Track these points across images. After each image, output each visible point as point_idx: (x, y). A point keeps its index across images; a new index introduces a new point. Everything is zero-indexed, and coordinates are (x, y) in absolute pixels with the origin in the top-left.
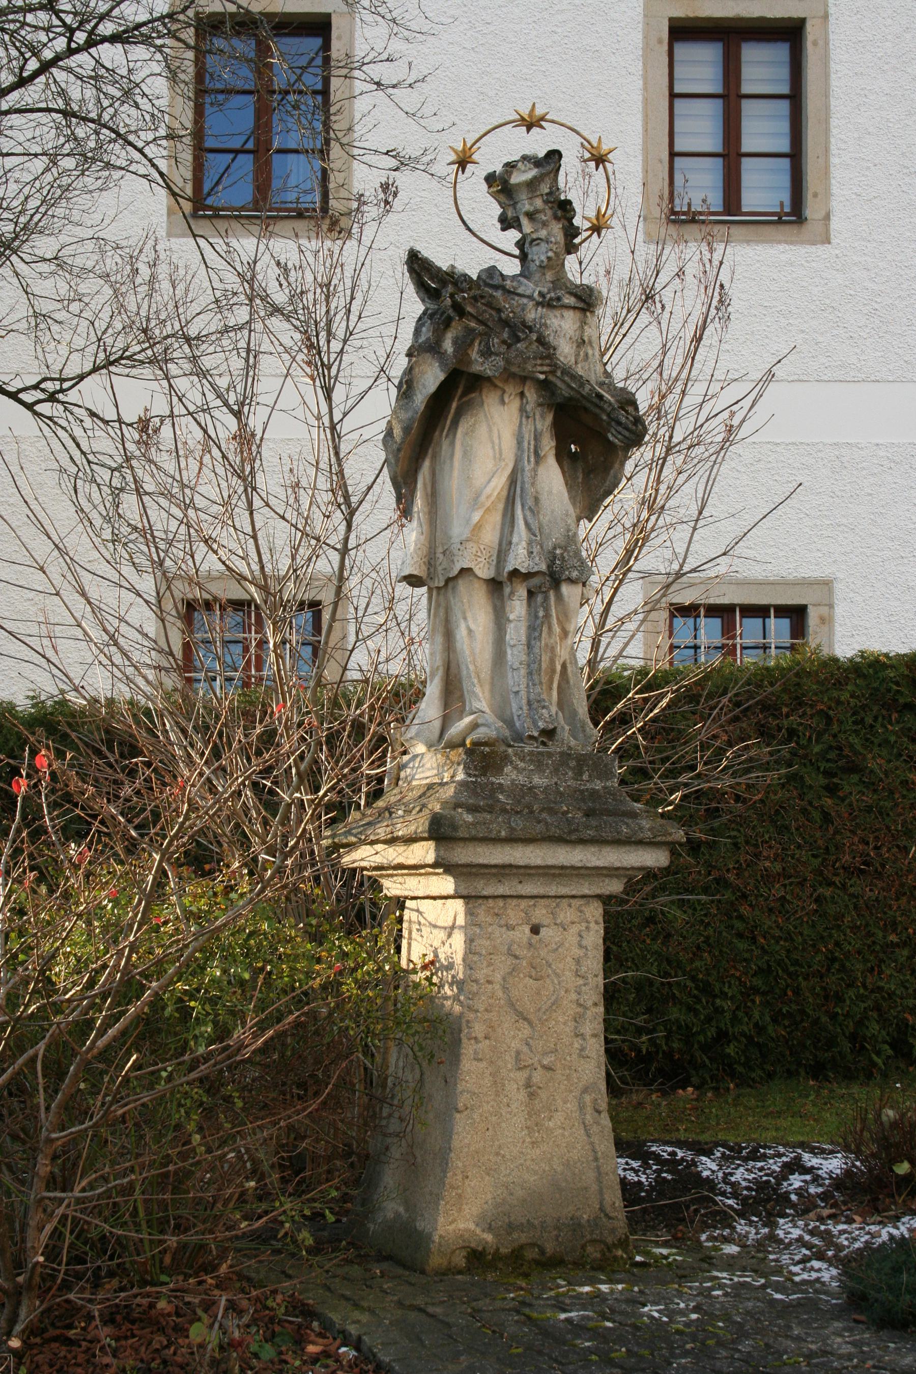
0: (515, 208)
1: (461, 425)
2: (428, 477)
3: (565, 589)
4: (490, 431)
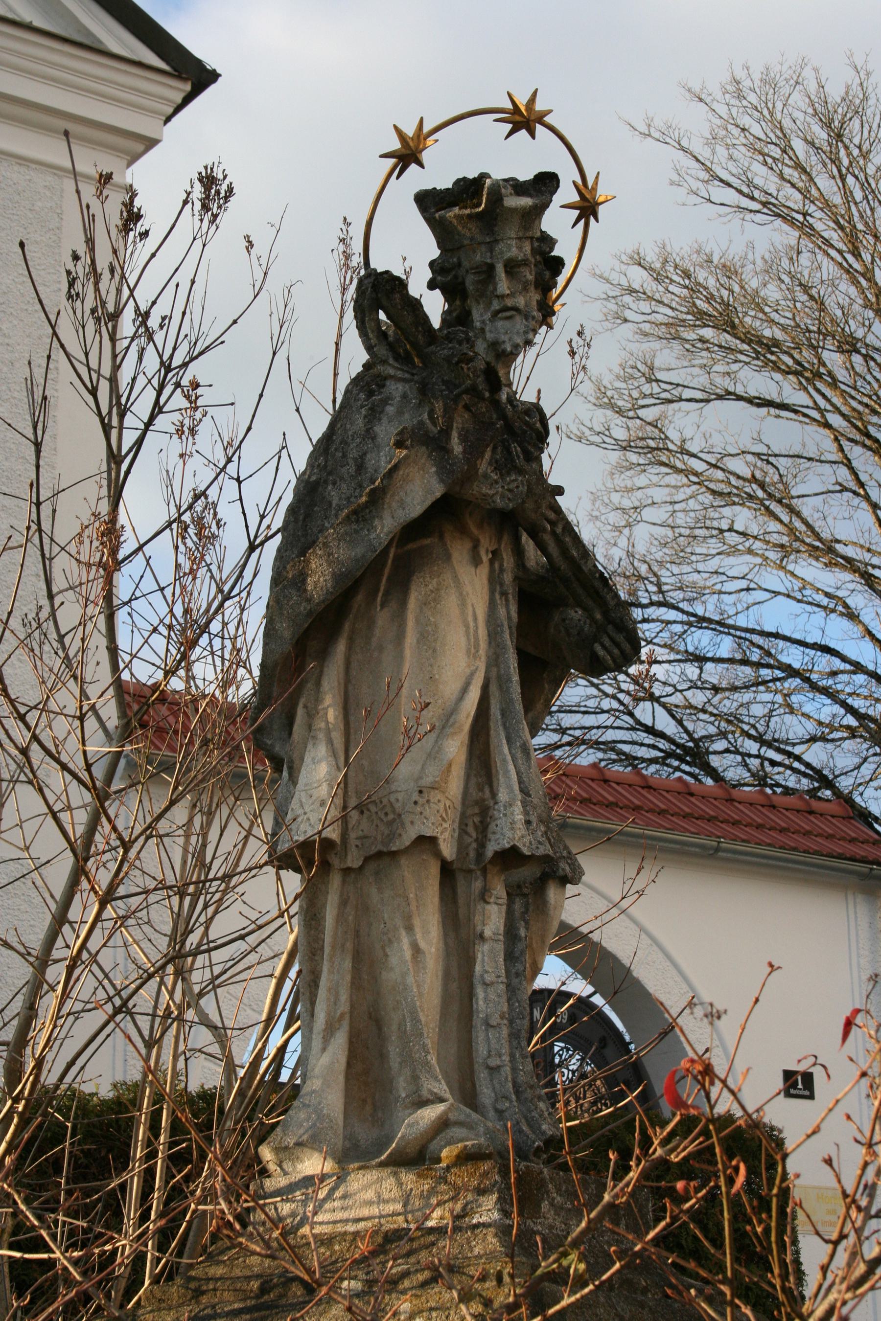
0: (491, 251)
4: (463, 604)
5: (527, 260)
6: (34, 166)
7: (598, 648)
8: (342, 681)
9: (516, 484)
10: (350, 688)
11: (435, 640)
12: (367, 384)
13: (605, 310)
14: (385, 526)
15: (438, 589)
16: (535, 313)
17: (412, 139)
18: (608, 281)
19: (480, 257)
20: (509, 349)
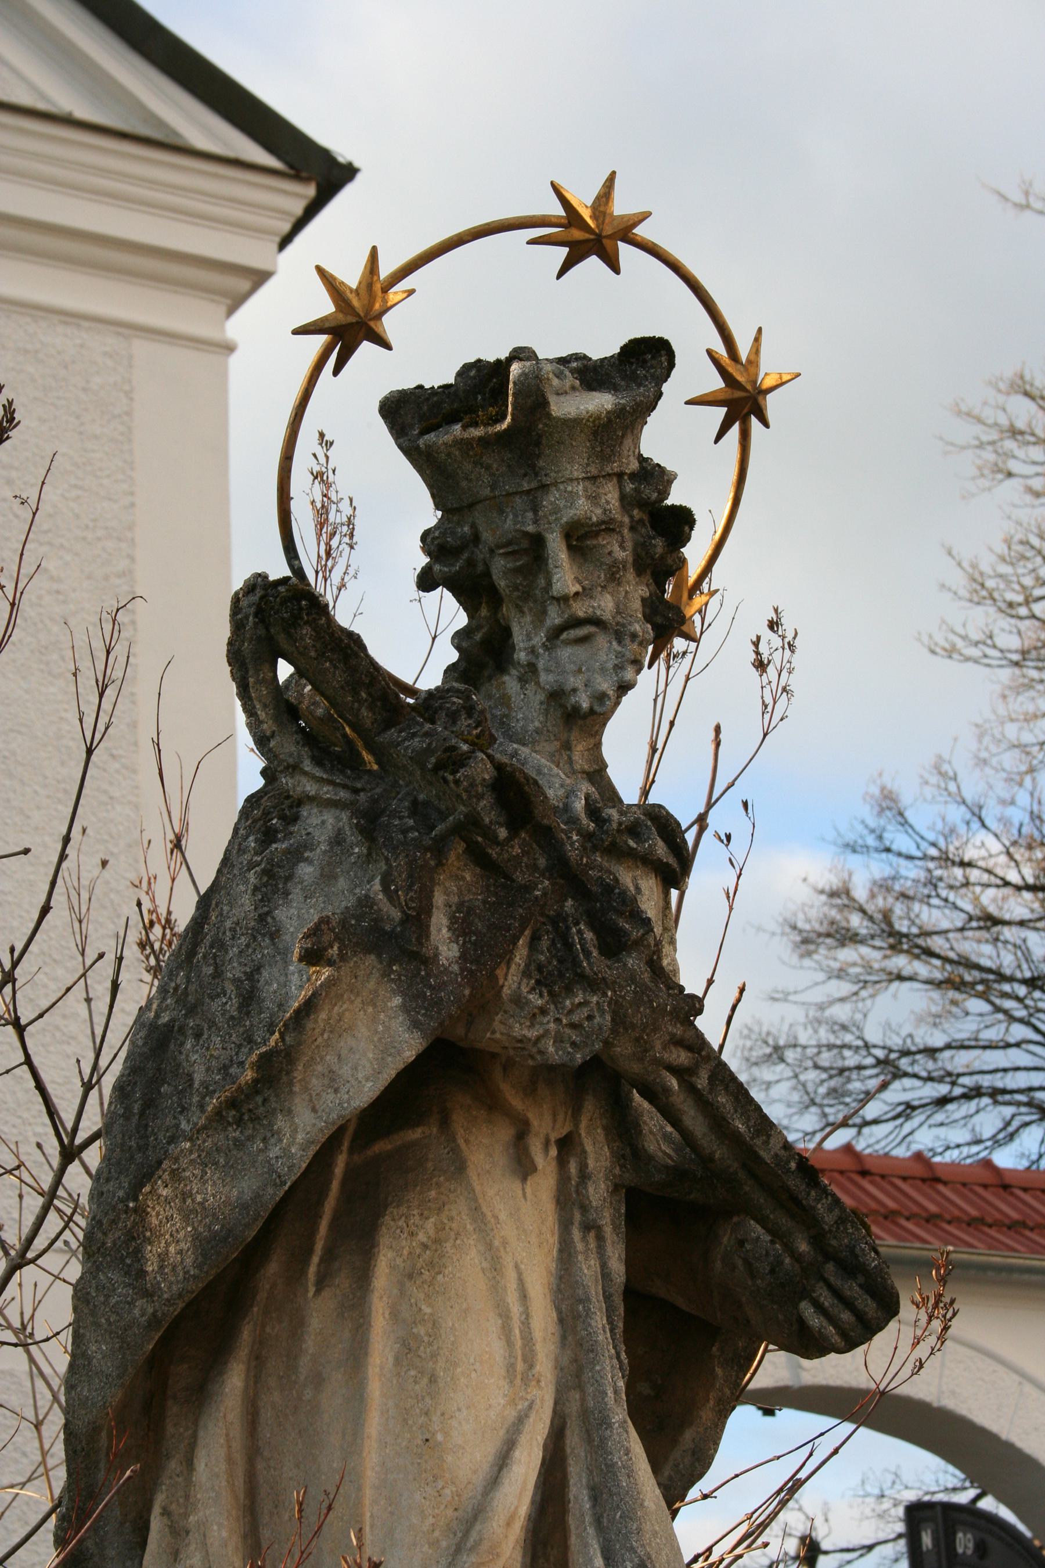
0: (535, 509)
1: (384, 1240)
2: (237, 1431)
4: (495, 1267)
5: (612, 520)
6: (86, 324)
7: (807, 1310)
8: (239, 1457)
9: (585, 1012)
10: (260, 1465)
11: (434, 1356)
12: (266, 818)
13: (979, 462)
14: (300, 1128)
15: (437, 1241)
16: (637, 627)
17: (357, 292)
18: (980, 421)
19: (515, 521)
20: (585, 705)
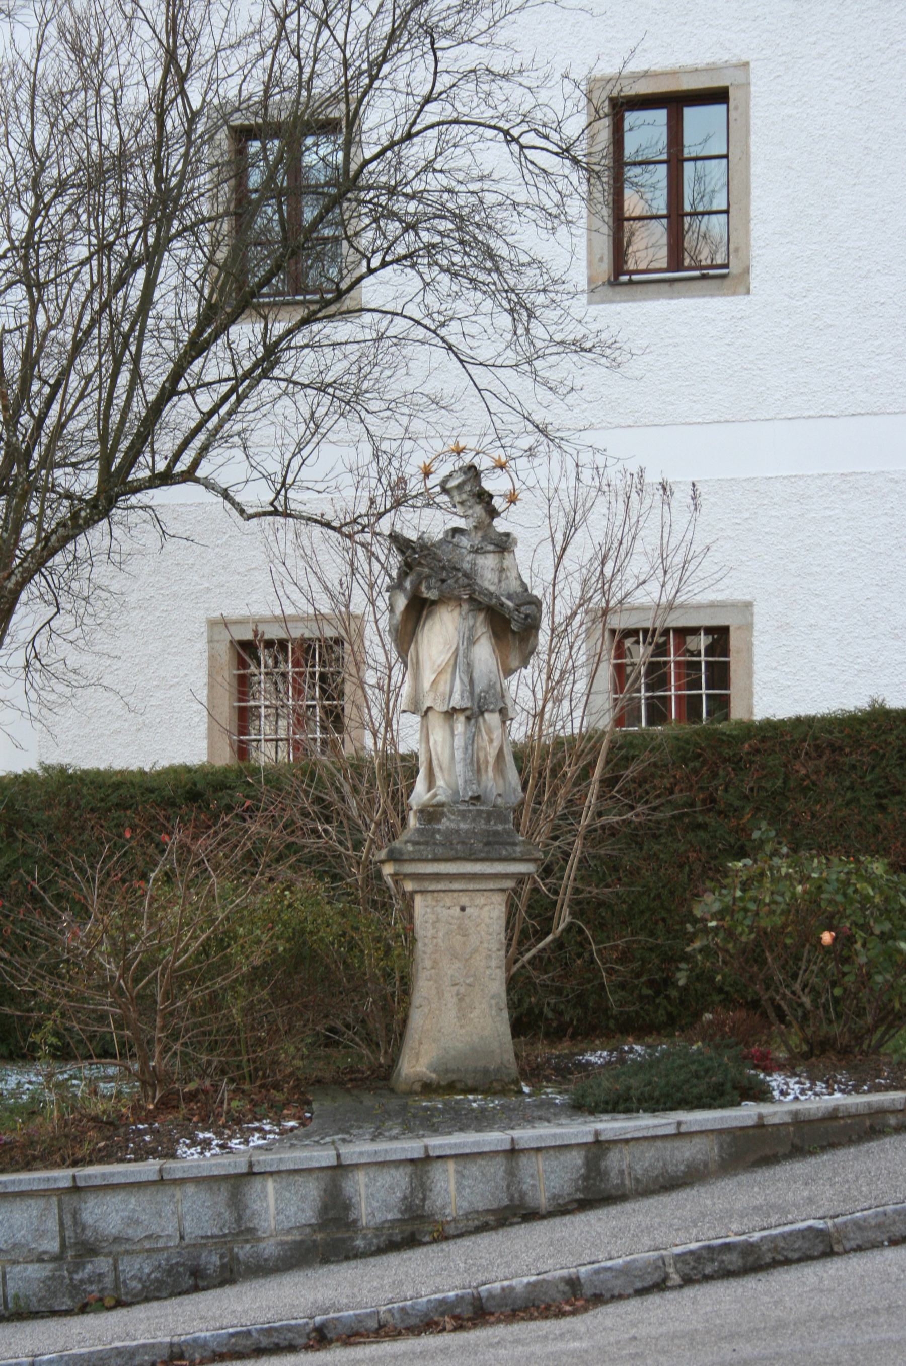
3: (486, 715)
